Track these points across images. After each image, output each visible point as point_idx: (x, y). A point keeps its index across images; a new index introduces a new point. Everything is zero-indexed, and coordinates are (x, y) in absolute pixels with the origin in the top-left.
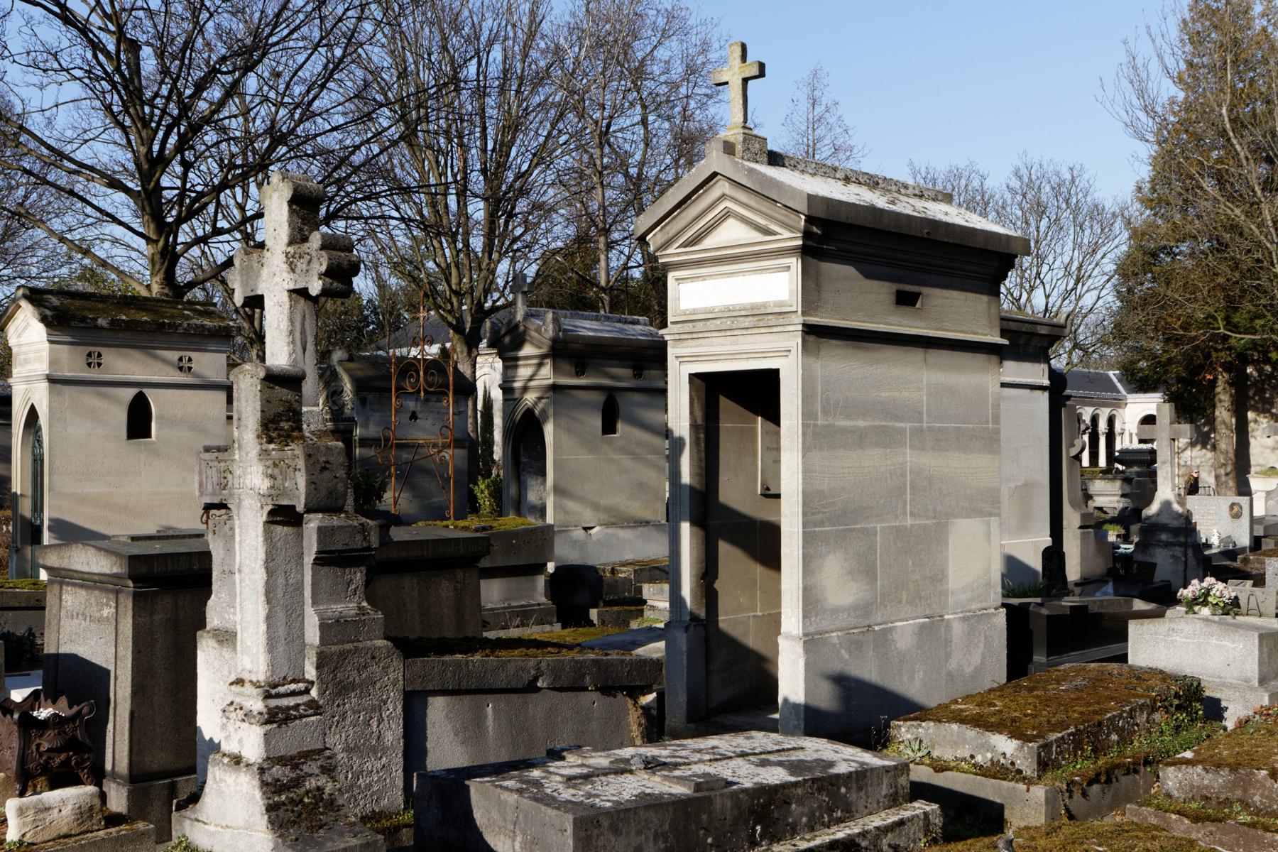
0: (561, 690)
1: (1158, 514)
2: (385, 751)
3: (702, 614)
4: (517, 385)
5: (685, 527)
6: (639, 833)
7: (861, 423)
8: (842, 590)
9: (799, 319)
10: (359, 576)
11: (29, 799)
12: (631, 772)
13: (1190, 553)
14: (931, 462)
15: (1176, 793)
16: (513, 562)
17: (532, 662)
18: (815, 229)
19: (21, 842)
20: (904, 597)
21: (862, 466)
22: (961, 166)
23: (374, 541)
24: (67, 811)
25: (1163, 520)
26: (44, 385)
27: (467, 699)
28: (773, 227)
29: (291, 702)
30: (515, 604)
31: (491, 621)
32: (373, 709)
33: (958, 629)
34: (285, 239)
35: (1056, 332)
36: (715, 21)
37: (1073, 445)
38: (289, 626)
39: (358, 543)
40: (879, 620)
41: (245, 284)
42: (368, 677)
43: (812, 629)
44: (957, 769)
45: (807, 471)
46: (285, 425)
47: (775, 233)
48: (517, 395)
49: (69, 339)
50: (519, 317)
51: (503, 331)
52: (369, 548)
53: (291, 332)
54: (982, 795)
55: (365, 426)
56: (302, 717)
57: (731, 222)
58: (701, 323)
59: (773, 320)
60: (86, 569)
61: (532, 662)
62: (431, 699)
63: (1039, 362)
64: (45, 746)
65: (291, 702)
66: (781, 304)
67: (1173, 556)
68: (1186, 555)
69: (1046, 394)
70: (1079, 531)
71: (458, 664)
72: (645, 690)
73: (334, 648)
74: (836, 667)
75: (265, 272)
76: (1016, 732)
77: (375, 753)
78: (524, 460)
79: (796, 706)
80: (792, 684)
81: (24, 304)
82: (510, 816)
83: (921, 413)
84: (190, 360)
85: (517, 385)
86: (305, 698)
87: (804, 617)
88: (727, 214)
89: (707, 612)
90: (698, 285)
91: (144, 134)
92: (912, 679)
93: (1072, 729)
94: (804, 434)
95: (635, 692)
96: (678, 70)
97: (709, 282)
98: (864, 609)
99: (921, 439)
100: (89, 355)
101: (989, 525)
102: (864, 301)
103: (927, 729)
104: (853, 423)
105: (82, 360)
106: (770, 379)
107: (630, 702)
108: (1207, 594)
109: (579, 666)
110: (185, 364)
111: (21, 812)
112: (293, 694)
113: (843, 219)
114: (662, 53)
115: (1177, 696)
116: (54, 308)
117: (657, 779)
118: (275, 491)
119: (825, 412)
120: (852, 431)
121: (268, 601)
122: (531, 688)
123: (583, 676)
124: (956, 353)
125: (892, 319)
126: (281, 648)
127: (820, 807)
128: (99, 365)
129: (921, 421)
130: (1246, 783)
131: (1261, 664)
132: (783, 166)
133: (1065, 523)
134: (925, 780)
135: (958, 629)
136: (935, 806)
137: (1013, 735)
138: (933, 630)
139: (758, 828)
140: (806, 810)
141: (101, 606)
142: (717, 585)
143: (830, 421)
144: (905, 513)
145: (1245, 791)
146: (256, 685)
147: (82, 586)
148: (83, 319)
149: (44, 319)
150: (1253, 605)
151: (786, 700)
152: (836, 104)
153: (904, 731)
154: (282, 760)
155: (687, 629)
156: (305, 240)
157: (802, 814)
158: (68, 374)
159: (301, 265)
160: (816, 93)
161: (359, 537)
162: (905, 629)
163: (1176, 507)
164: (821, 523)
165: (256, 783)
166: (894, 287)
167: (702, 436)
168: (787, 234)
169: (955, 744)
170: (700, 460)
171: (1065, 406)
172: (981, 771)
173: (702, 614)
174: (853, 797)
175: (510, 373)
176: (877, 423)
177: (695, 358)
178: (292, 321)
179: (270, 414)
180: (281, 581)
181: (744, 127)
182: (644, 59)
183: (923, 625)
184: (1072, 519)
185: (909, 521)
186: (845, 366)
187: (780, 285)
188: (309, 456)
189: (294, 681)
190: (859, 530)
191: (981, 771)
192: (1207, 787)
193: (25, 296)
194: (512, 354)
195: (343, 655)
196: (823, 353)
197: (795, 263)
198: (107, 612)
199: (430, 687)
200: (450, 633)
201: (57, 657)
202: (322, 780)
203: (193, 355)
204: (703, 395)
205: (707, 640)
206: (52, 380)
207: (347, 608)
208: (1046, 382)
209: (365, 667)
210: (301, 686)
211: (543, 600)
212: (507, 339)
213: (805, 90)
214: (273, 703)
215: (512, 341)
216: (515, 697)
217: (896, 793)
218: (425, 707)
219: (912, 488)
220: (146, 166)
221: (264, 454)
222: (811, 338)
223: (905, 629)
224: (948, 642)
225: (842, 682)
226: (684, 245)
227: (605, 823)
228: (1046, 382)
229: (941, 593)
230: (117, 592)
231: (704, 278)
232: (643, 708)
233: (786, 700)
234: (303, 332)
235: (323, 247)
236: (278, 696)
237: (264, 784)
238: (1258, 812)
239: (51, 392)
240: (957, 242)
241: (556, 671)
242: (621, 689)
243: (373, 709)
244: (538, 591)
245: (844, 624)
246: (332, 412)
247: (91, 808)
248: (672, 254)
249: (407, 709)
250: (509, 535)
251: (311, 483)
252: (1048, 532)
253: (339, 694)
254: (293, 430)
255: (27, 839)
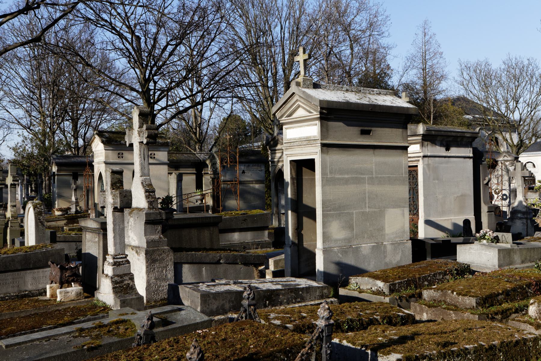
0: (229, 264)
1: (517, 206)
2: (168, 280)
3: (296, 242)
4: (276, 160)
5: (290, 212)
6: (223, 300)
7: (346, 176)
8: (338, 232)
9: (319, 142)
10: (159, 228)
11: (63, 290)
12: (230, 285)
13: (529, 221)
14: (377, 189)
15: (426, 299)
16: (255, 226)
17: (218, 255)
18: (324, 111)
19: (60, 301)
20: (366, 236)
21: (342, 192)
22: (482, 60)
23: (164, 217)
24: (73, 293)
25: (519, 209)
26: (104, 165)
27: (196, 265)
28: (312, 111)
29: (121, 260)
30: (256, 241)
31: (247, 247)
32: (164, 267)
33: (389, 248)
34: (138, 127)
35: (475, 135)
36: (380, 4)
37: (485, 180)
38: (120, 240)
39: (159, 217)
40: (355, 244)
41: (129, 140)
42: (162, 258)
43: (326, 246)
44: (366, 292)
45: (324, 193)
46: (118, 185)
47: (312, 113)
48: (276, 164)
49: (112, 148)
50: (275, 134)
51: (270, 140)
52: (162, 219)
53: (140, 155)
54: (354, 296)
55: (225, 176)
56: (124, 264)
57: (300, 109)
58: (293, 143)
59: (312, 142)
60: (91, 227)
61: (218, 255)
62: (184, 265)
63: (468, 147)
64: (67, 275)
65: (121, 260)
66: (314, 137)
67: (523, 223)
68: (527, 222)
69: (472, 160)
70: (487, 213)
71: (192, 255)
72: (261, 265)
73: (151, 249)
74: (337, 259)
75: (133, 136)
76: (385, 280)
77: (165, 280)
78: (279, 188)
79: (321, 272)
80: (320, 266)
81: (96, 136)
82: (187, 295)
83: (372, 172)
84: (154, 154)
85: (276, 160)
86: (125, 259)
87: (323, 242)
88: (299, 106)
89: (298, 241)
90: (292, 130)
91: (142, 70)
92: (369, 264)
93: (406, 279)
94: (322, 180)
95: (257, 265)
96: (364, 25)
97: (295, 129)
98: (349, 240)
99: (372, 181)
100: (119, 154)
101: (403, 211)
102: (348, 134)
103: (359, 279)
104: (344, 176)
105: (116, 156)
106: (313, 161)
107: (254, 269)
108: (485, 235)
109: (235, 257)
110: (153, 156)
111: (61, 293)
112: (121, 258)
113: (334, 107)
114: (358, 19)
115: (456, 270)
116: (107, 138)
117: (236, 286)
118: (114, 203)
119: (331, 173)
120: (343, 179)
121: (114, 233)
122: (218, 263)
123: (237, 260)
124: (387, 150)
125: (359, 140)
126: (118, 246)
127: (291, 297)
128: (122, 157)
129: (373, 174)
130: (445, 295)
131: (499, 260)
132: (320, 88)
133: (482, 210)
134: (357, 296)
135: (389, 248)
136: (336, 300)
137: (383, 281)
138: (378, 248)
139: (267, 302)
140: (286, 298)
141: (95, 238)
142: (303, 232)
143: (333, 176)
144: (366, 207)
145: (445, 297)
146: (111, 255)
147: (91, 232)
148: (116, 141)
149: (102, 142)
150: (504, 239)
151: (318, 270)
152: (434, 34)
153: (353, 280)
154: (118, 276)
155: (290, 247)
156: (142, 127)
157: (284, 299)
158: (111, 161)
159: (141, 135)
160: (426, 30)
161: (159, 216)
162: (366, 247)
163: (524, 203)
164: (330, 211)
165: (110, 281)
166: (360, 128)
167: (295, 181)
168: (315, 113)
169: (367, 284)
170: (295, 189)
171: (482, 164)
172: (374, 293)
173: (296, 242)
174: (305, 295)
175: (273, 155)
176: (354, 176)
177: (291, 155)
178: (140, 151)
179: (113, 182)
180: (118, 227)
181: (304, 76)
182: (351, 22)
183: (374, 246)
184: (484, 209)
185: (367, 210)
186: (339, 158)
187: (313, 130)
188: (120, 193)
189: (122, 255)
190: (346, 213)
191: (374, 293)
192: (435, 297)
193: (97, 134)
194: (274, 148)
195: (154, 251)
196: (329, 153)
197: (318, 122)
198: (97, 240)
199: (183, 261)
200: (197, 246)
201: (85, 253)
202: (129, 282)
203: (155, 152)
204: (295, 167)
205: (298, 251)
206: (106, 163)
207: (156, 237)
208: (471, 155)
209: (161, 255)
210: (124, 256)
211: (267, 239)
212: (272, 143)
213: (421, 29)
214: (116, 260)
215: (273, 143)
216: (213, 265)
217: (323, 295)
218: (182, 267)
219: (369, 198)
220: (143, 82)
221: (112, 192)
222: (325, 148)
223: (366, 247)
224: (385, 252)
225: (340, 265)
226: (287, 117)
227: (211, 296)
228: (471, 155)
229: (382, 235)
230: (99, 234)
231: (301, 126)
232: (259, 270)
233: (318, 270)
234: (144, 154)
235: (147, 129)
236: (117, 258)
237: (112, 282)
238: (448, 305)
239: (106, 167)
240: (384, 111)
241: (227, 258)
242: (252, 264)
243: (164, 267)
244: (265, 236)
245: (340, 245)
246: (213, 171)
247: (80, 293)
248: (283, 120)
249: (175, 268)
250: (253, 216)
251: (121, 201)
252: (473, 214)
253: (153, 262)
254: (120, 186)
255: (62, 300)
